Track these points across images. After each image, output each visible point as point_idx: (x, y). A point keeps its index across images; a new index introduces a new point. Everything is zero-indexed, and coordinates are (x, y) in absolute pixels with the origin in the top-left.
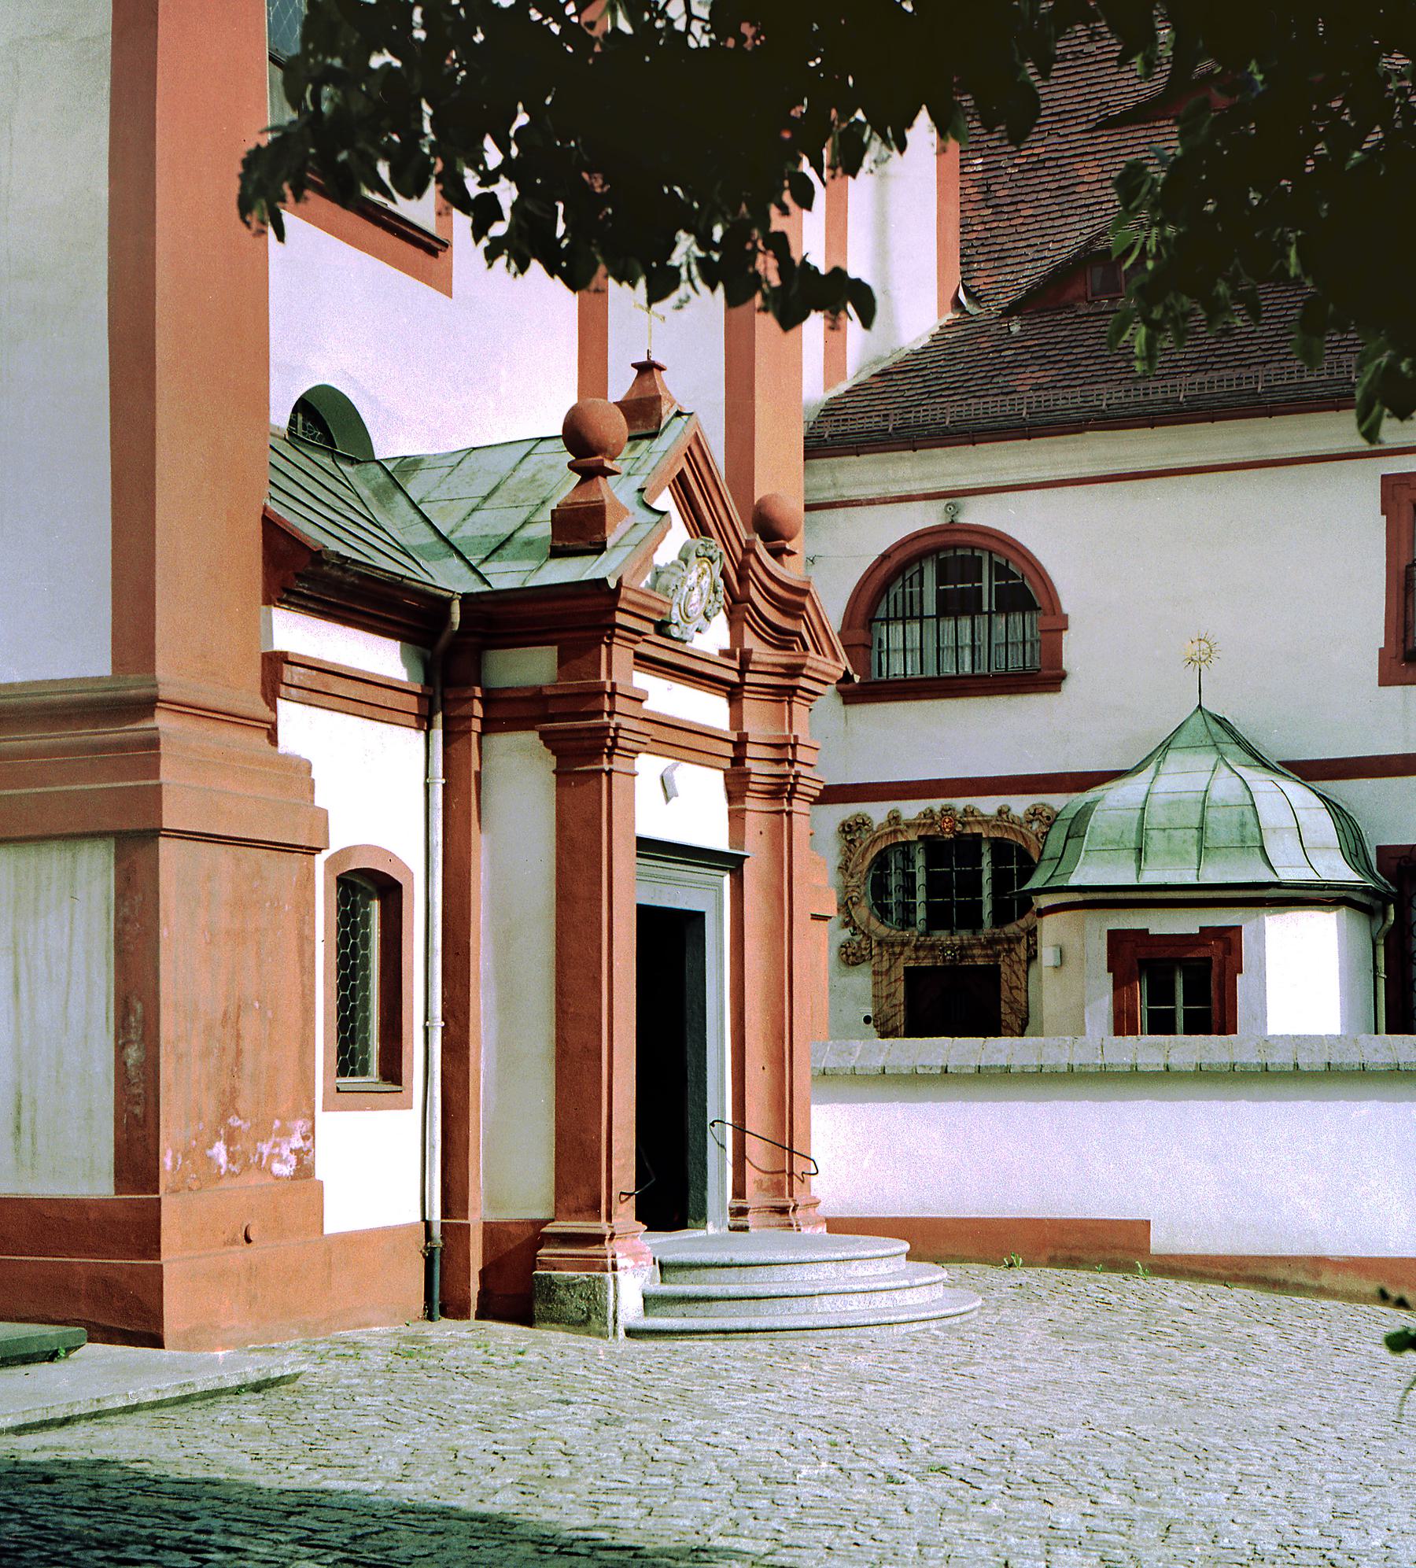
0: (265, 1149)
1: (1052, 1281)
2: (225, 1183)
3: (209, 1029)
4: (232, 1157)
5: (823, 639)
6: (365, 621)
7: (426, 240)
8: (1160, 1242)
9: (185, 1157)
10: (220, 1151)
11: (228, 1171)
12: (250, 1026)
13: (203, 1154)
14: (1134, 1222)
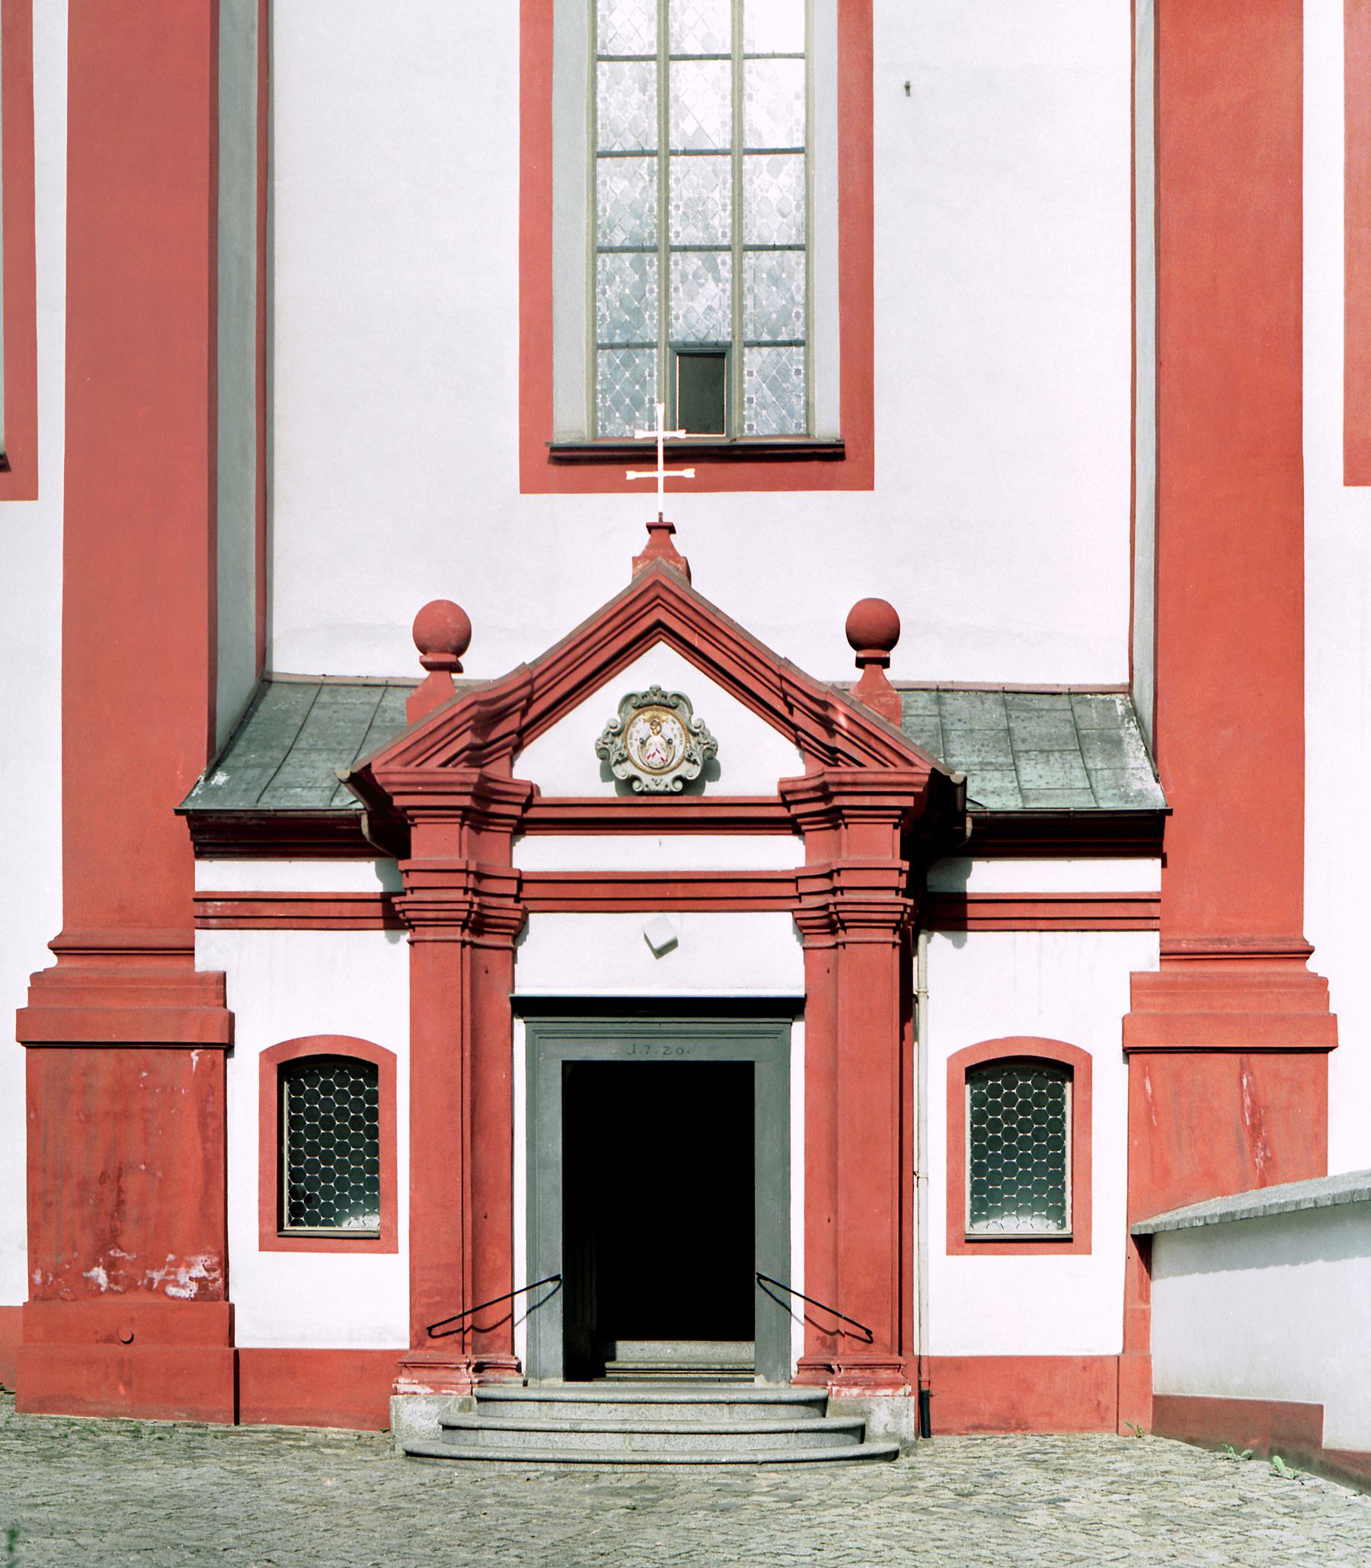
0: (157, 1276)
1: (1193, 1467)
2: (102, 1299)
3: (83, 1185)
4: (112, 1279)
5: (873, 743)
6: (345, 850)
7: (808, 451)
8: (1336, 1435)
9: (56, 1276)
10: (100, 1275)
11: (109, 1290)
12: (132, 1184)
13: (79, 1274)
14: (1308, 1406)
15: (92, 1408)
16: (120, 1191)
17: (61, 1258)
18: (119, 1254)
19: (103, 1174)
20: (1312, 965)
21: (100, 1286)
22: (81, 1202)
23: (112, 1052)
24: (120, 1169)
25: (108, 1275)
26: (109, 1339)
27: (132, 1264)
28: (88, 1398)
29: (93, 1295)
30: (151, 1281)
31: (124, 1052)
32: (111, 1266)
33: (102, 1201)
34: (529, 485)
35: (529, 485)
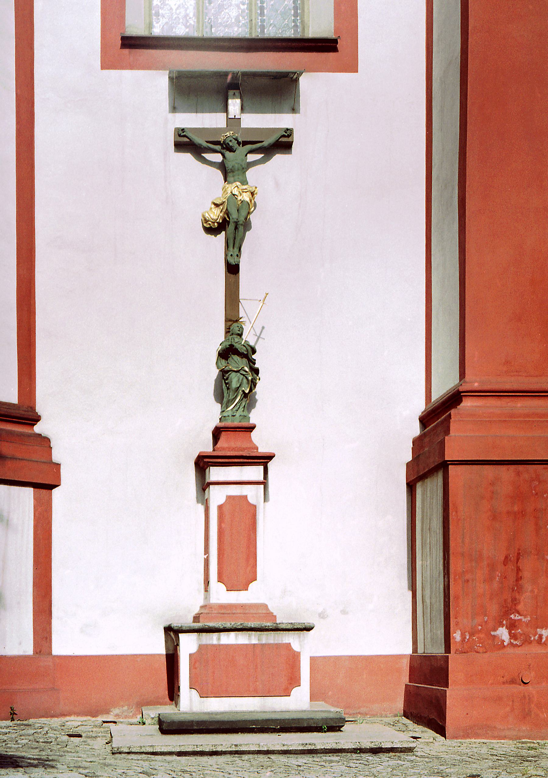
3: (492, 567)
4: (513, 636)
9: (472, 634)
10: (503, 633)
11: (511, 644)
15: (503, 734)
16: (518, 569)
17: (476, 621)
18: (518, 617)
19: (506, 557)
20: (38, 429)
21: (504, 641)
22: (489, 579)
23: (512, 467)
24: (519, 554)
25: (510, 633)
26: (513, 682)
27: (527, 625)
28: (499, 726)
29: (499, 649)
30: (541, 636)
31: (521, 468)
32: (512, 626)
33: (505, 577)
34: (108, 63)
35: (108, 63)
